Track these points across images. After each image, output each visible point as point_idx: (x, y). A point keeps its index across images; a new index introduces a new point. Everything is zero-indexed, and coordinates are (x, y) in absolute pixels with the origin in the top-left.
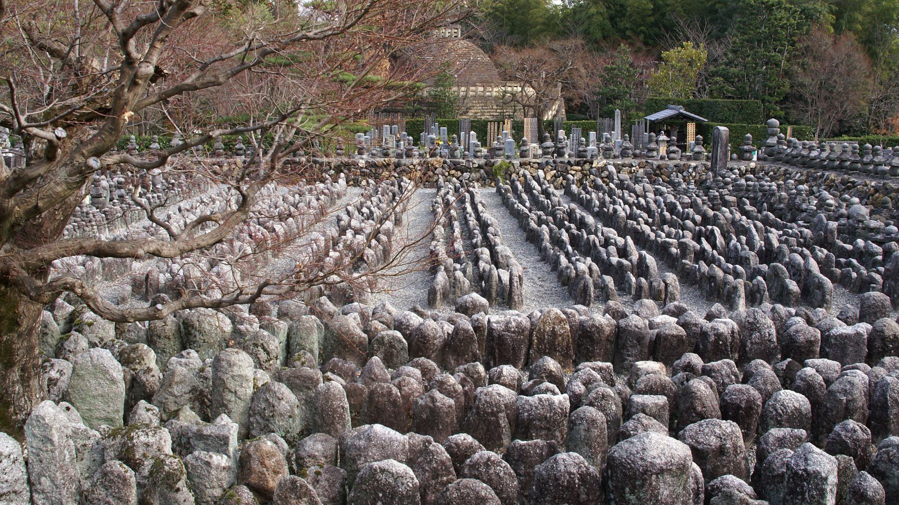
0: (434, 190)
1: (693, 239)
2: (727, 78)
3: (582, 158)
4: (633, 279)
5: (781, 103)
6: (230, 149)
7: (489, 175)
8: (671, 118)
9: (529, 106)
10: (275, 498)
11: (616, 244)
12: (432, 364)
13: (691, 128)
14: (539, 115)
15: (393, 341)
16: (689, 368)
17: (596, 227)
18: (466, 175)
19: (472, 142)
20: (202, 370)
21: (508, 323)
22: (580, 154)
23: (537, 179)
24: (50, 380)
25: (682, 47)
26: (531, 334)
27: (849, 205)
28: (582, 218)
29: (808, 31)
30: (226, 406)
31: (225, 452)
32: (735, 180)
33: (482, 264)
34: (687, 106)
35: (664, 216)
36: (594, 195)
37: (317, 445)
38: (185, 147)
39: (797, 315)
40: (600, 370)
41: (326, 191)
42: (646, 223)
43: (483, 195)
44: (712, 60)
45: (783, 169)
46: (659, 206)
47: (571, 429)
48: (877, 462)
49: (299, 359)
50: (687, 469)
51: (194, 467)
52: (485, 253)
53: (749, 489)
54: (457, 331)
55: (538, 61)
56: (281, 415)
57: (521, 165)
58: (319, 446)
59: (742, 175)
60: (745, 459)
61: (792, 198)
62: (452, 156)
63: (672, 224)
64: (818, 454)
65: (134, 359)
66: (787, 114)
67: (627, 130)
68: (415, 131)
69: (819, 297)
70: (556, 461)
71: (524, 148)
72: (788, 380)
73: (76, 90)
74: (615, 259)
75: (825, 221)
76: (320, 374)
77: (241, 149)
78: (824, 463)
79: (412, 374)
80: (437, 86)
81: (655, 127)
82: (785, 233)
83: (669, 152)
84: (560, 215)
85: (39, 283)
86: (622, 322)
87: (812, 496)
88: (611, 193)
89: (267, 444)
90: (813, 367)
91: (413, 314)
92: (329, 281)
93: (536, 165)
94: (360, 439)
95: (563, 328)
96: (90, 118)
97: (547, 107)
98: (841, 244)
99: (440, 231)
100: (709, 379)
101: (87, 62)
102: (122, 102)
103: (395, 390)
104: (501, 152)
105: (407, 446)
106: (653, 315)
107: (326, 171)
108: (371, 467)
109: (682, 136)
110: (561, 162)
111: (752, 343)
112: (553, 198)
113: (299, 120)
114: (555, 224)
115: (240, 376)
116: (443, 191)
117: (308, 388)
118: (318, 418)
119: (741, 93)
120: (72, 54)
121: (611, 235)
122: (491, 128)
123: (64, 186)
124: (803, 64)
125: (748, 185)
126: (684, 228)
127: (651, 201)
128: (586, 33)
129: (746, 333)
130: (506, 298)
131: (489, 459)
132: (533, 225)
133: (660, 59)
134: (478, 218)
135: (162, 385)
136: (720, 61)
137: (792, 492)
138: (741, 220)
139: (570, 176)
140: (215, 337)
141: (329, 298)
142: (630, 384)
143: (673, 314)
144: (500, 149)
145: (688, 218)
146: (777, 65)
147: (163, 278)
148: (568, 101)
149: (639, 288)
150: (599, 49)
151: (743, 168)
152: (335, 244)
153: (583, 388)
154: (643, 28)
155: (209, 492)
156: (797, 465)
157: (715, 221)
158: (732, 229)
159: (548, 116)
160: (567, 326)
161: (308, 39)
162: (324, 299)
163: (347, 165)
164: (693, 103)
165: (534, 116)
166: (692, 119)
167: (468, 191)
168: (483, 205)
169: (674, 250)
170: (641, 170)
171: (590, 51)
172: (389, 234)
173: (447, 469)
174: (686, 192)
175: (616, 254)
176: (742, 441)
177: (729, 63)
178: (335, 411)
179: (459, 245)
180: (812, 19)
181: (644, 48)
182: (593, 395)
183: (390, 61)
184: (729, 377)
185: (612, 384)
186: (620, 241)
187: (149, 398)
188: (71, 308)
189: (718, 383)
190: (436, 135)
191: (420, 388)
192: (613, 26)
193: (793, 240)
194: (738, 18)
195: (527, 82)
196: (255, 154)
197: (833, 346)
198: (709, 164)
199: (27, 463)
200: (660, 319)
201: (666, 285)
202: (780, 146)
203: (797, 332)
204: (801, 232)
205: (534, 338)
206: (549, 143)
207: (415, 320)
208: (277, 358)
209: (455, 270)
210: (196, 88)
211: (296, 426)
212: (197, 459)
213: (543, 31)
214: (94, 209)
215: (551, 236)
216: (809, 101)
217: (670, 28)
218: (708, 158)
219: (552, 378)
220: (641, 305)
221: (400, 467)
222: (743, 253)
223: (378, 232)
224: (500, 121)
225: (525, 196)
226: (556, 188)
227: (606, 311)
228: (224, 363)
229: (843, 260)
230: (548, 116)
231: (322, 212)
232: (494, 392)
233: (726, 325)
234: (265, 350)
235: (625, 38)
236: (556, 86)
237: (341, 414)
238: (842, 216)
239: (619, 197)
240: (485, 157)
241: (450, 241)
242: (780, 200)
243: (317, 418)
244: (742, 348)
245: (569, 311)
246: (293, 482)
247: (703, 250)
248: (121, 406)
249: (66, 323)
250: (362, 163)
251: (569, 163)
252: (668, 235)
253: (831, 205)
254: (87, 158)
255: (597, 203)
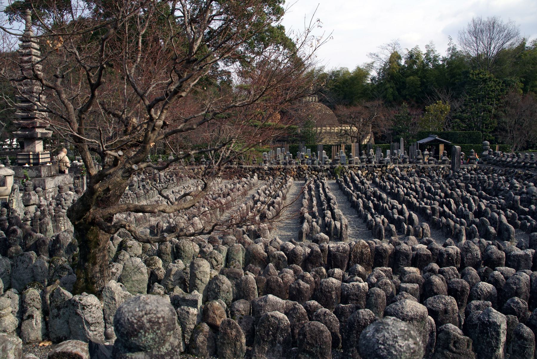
0: (304, 182)
1: (439, 206)
2: (462, 120)
3: (382, 164)
4: (406, 226)
5: (493, 132)
6: (198, 161)
7: (332, 173)
8: (431, 142)
9: (354, 137)
10: (220, 329)
11: (397, 208)
12: (299, 268)
13: (441, 147)
14: (359, 141)
15: (280, 257)
16: (432, 271)
17: (387, 200)
18: (321, 174)
19: (324, 156)
20: (185, 269)
21: (338, 247)
22: (380, 162)
23: (357, 175)
24: (112, 273)
25: (437, 103)
26: (350, 254)
27: (528, 187)
28: (380, 195)
29: (507, 93)
30: (196, 287)
31: (197, 307)
32: (465, 174)
33: (326, 219)
34: (440, 135)
35: (424, 194)
36: (387, 183)
37: (242, 306)
38: (177, 160)
39: (493, 244)
40: (385, 271)
41: (247, 182)
42: (415, 197)
43: (329, 184)
44: (453, 110)
45: (492, 168)
46: (422, 189)
47: (367, 299)
48: (530, 319)
49: (233, 265)
50: (425, 318)
51: (181, 314)
52: (329, 213)
53: (460, 331)
54: (312, 251)
55: (359, 113)
56: (223, 291)
57: (350, 168)
58: (242, 306)
59: (469, 171)
60: (459, 316)
61: (496, 183)
62: (313, 163)
63: (428, 198)
64: (495, 312)
65: (152, 264)
66: (496, 138)
67: (407, 149)
68: (294, 152)
69: (507, 236)
70: (359, 313)
71: (351, 159)
72: (484, 278)
73: (125, 133)
74: (396, 216)
75: (513, 195)
76: (243, 271)
77: (204, 161)
78: (499, 318)
79: (289, 273)
80: (305, 127)
81: (422, 147)
82: (491, 202)
83: (429, 160)
84: (369, 193)
85: (109, 224)
86: (398, 247)
87: (493, 335)
88: (397, 182)
89: (217, 303)
90: (500, 271)
91: (290, 243)
92: (248, 226)
93: (357, 168)
94: (262, 302)
95: (367, 250)
96: (133, 146)
97: (364, 137)
98: (522, 208)
99: (305, 202)
100: (441, 276)
101: (130, 119)
102: (148, 138)
103: (280, 280)
104: (339, 161)
105: (285, 305)
106: (415, 244)
107: (247, 173)
108: (267, 315)
109: (437, 151)
110: (370, 166)
111: (467, 259)
112: (365, 185)
113: (232, 146)
114: (366, 198)
115: (203, 272)
116: (308, 182)
117: (237, 278)
118: (242, 292)
119: (470, 128)
120: (123, 116)
121: (395, 204)
122: (334, 149)
123: (121, 178)
124: (505, 111)
125: (472, 177)
126: (434, 200)
127: (418, 186)
128: (384, 97)
129: (464, 253)
130: (337, 236)
131: (325, 312)
132: (354, 199)
133: (425, 110)
134: (326, 195)
135: (165, 276)
136: (458, 111)
137: (482, 332)
138: (466, 195)
139: (375, 174)
140: (190, 255)
141: (248, 235)
142: (401, 279)
143: (425, 244)
144: (338, 160)
145: (437, 195)
146: (490, 112)
147: (165, 226)
148: (375, 134)
149: (409, 230)
150: (392, 106)
151: (470, 168)
152: (252, 209)
153: (376, 280)
154: (415, 94)
155: (188, 326)
156: (484, 318)
157: (451, 196)
158: (461, 200)
159: (365, 142)
160: (369, 250)
161: (236, 107)
162: (245, 236)
163: (258, 169)
164: (443, 133)
165: (357, 142)
166: (442, 142)
167: (321, 182)
168: (329, 189)
169: (429, 211)
170: (414, 170)
171: (387, 107)
172: (279, 204)
173: (304, 317)
174: (437, 181)
175: (397, 213)
176: (457, 307)
177: (463, 112)
178: (250, 290)
179: (315, 209)
180: (509, 86)
181: (416, 105)
182: (380, 283)
183: (280, 114)
184: (453, 275)
185: (391, 278)
186: (400, 206)
187: (159, 282)
188: (121, 239)
189: (447, 278)
190: (305, 153)
191: (293, 279)
192: (399, 94)
193: (494, 206)
194: (467, 87)
195: (353, 124)
196: (211, 163)
197: (512, 261)
198: (450, 166)
199: (103, 310)
200: (419, 246)
201: (423, 229)
202: (490, 156)
203: (492, 253)
204: (499, 202)
205: (352, 255)
206: (363, 156)
207: (291, 246)
208: (221, 264)
209: (313, 221)
210: (183, 131)
211: (231, 297)
212: (183, 310)
213: (361, 97)
214: (130, 192)
215: (363, 205)
216: (509, 131)
217: (431, 94)
218: (450, 163)
219: (360, 275)
220: (408, 239)
221: (281, 315)
222: (465, 213)
223: (273, 202)
224: (339, 146)
225: (351, 184)
226: (368, 180)
227: (390, 242)
228: (196, 265)
229: (523, 216)
230: (365, 142)
231: (245, 194)
232: (330, 281)
233: (454, 249)
234: (216, 260)
235: (405, 99)
236: (369, 126)
237: (253, 291)
238: (523, 193)
239: (401, 184)
240: (330, 164)
241: (311, 207)
242: (489, 184)
243: (241, 293)
244: (462, 262)
245: (370, 241)
246: (229, 322)
247: (444, 211)
248: (146, 285)
249: (118, 247)
250: (266, 168)
251: (375, 167)
252: (426, 204)
253: (517, 187)
254: (131, 165)
255: (389, 187)
